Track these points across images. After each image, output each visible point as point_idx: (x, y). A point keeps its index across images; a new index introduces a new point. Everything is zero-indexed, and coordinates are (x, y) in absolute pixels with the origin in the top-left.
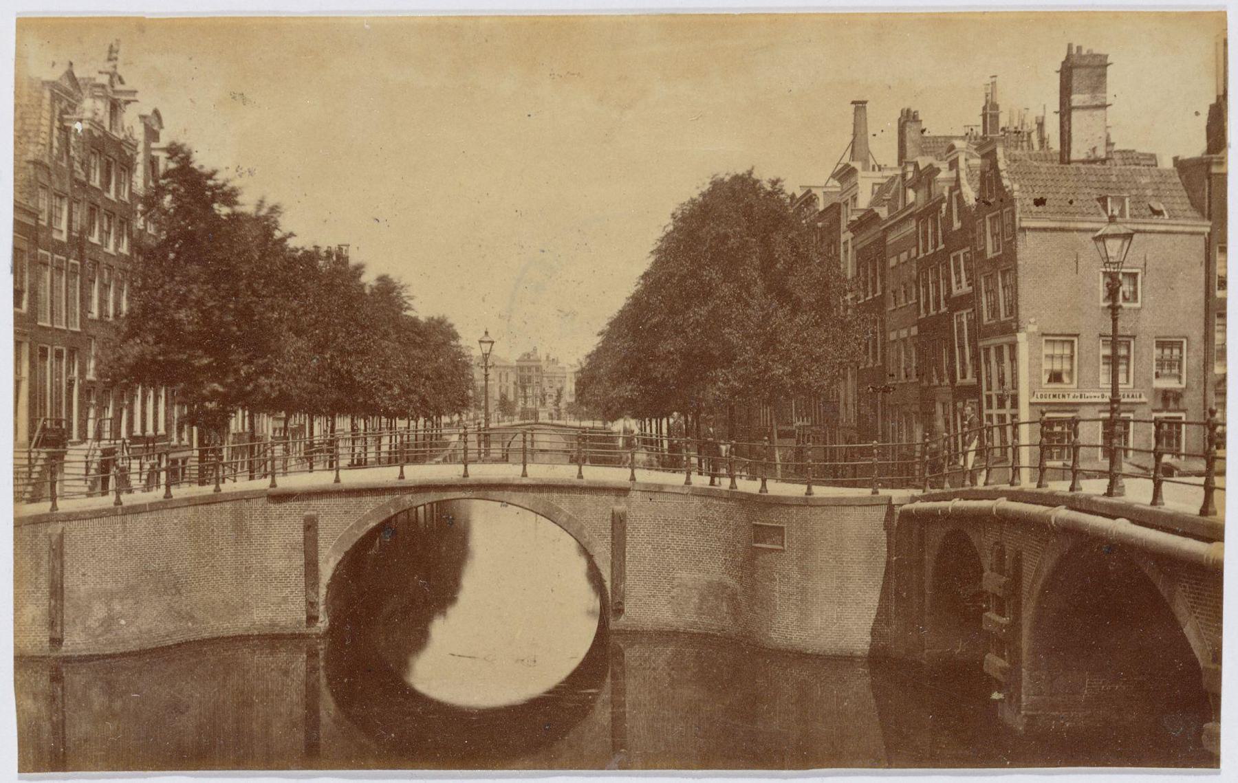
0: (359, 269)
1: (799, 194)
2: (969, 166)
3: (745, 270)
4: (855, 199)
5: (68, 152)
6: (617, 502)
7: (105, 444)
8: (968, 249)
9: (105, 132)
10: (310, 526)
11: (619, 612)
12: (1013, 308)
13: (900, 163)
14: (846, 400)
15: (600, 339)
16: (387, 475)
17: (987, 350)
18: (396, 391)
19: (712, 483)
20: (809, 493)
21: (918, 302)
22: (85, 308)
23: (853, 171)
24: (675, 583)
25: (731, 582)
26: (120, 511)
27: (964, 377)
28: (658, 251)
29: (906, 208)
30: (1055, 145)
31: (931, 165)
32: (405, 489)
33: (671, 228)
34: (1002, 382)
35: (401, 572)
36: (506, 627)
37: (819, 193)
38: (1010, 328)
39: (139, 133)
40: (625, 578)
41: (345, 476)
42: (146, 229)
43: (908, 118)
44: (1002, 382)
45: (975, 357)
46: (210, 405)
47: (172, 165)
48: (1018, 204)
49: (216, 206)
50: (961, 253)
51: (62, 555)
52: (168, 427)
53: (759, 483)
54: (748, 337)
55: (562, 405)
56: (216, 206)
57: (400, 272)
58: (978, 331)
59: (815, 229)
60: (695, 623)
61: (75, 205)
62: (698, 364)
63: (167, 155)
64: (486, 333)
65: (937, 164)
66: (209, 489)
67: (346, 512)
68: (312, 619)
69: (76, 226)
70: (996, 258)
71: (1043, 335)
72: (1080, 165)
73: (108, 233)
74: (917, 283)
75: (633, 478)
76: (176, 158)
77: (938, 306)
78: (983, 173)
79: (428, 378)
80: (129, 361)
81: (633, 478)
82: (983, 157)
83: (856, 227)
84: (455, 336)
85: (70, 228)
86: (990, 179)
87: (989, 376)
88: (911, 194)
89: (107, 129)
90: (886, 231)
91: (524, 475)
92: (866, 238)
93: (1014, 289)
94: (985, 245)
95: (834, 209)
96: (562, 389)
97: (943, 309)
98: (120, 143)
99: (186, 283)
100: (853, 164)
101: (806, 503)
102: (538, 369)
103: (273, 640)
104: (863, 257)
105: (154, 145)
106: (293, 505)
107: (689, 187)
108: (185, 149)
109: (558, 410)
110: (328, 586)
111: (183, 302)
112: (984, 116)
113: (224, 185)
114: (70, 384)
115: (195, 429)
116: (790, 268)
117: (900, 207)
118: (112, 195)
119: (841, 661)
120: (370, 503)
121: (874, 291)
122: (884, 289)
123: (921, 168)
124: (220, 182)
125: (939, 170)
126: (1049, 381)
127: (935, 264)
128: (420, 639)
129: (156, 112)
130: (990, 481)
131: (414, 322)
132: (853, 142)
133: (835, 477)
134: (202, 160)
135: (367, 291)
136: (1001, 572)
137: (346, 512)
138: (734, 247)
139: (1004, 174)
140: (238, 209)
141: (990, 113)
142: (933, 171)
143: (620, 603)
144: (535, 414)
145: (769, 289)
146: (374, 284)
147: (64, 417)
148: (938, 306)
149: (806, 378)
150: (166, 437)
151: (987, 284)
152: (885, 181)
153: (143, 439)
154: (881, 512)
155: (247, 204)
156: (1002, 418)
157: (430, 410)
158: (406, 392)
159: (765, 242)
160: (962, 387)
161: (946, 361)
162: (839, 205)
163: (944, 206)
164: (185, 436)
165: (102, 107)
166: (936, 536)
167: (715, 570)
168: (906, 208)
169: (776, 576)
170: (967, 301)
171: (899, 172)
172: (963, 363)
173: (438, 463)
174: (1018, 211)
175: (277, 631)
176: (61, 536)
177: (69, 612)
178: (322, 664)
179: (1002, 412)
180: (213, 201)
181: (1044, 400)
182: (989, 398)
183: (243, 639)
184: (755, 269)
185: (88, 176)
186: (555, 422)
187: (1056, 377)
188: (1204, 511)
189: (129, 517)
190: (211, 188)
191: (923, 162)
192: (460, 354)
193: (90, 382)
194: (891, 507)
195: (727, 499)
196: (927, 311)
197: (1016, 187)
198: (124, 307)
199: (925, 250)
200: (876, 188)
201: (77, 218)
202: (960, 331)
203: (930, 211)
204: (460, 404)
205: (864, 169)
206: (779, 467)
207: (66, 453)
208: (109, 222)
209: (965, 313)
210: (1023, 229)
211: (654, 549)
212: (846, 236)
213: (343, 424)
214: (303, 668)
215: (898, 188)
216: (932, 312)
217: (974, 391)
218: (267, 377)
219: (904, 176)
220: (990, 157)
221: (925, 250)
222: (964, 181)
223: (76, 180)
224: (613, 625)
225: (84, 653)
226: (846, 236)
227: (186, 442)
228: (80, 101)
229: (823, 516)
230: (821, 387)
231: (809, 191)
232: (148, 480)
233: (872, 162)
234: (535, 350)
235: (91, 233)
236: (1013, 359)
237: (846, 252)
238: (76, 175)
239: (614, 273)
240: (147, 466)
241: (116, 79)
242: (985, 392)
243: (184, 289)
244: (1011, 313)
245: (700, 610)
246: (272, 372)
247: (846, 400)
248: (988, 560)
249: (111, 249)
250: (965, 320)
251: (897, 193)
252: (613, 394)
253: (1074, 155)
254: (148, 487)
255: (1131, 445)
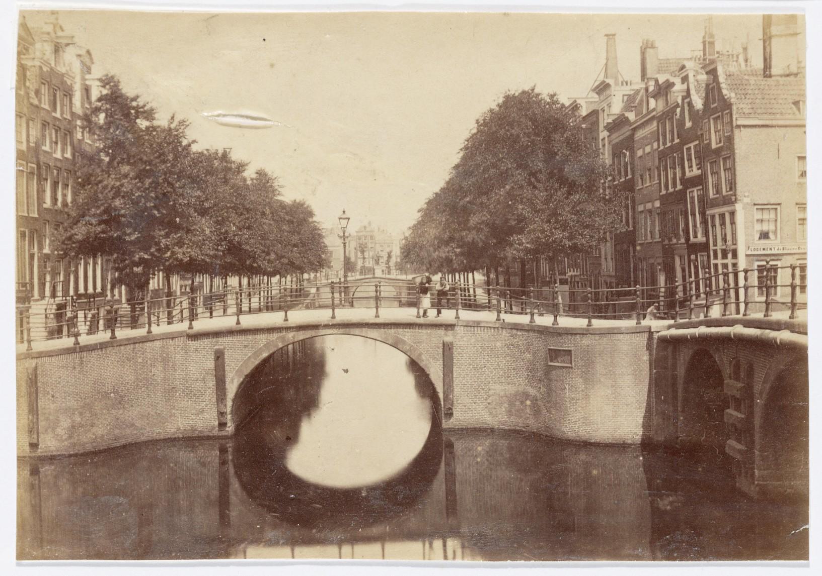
0: (241, 167)
1: (567, 104)
2: (697, 81)
3: (533, 162)
4: (609, 106)
5: (24, 84)
6: (446, 335)
7: (59, 300)
8: (697, 142)
9: (52, 69)
10: (219, 356)
11: (450, 415)
12: (732, 185)
13: (643, 80)
14: (606, 255)
15: (419, 214)
16: (274, 318)
17: (713, 217)
18: (273, 256)
19: (638, 323)
20: (589, 325)
21: (660, 183)
22: (41, 200)
23: (607, 86)
24: (491, 392)
25: (532, 392)
26: (78, 350)
27: (696, 237)
28: (466, 148)
29: (649, 112)
30: (759, 64)
31: (667, 80)
32: (288, 329)
33: (475, 131)
34: (724, 240)
35: (281, 390)
36: (358, 430)
37: (581, 102)
38: (729, 201)
39: (77, 67)
40: (453, 391)
41: (244, 322)
42: (83, 139)
43: (646, 47)
44: (724, 240)
45: (704, 222)
46: (138, 270)
47: (105, 92)
48: (734, 108)
49: (138, 121)
50: (692, 145)
51: (36, 383)
52: (104, 288)
53: (528, 317)
54: (537, 211)
55: (392, 263)
56: (138, 121)
57: (271, 169)
58: (705, 203)
59: (580, 128)
60: (506, 422)
61: (31, 123)
62: (502, 233)
63: (99, 83)
64: (344, 212)
65: (672, 80)
66: (141, 332)
67: (245, 346)
68: (222, 425)
69: (32, 139)
70: (719, 148)
71: (755, 204)
72: (779, 78)
73: (56, 143)
74: (658, 168)
75: (457, 317)
76: (108, 87)
77: (675, 185)
78: (707, 85)
79: (295, 246)
80: (79, 237)
81: (457, 317)
82: (707, 73)
83: (613, 127)
84: (311, 214)
85: (28, 141)
86: (712, 90)
87: (715, 237)
88: (652, 103)
89: (53, 65)
90: (635, 130)
91: (377, 316)
92: (617, 137)
93: (732, 170)
94: (710, 139)
95: (594, 114)
96: (391, 252)
97: (679, 187)
98: (63, 75)
99: (119, 179)
100: (608, 81)
101: (583, 333)
102: (372, 237)
103: (192, 440)
104: (617, 153)
105: (87, 76)
106: (206, 342)
107: (491, 101)
108: (115, 79)
109: (389, 268)
110: (233, 401)
111: (117, 193)
112: (704, 43)
113: (145, 106)
114: (32, 256)
115: (123, 287)
116: (566, 160)
117: (645, 112)
118: (58, 115)
119: (619, 447)
120: (262, 339)
121: (626, 175)
122: (633, 174)
123: (660, 83)
124: (141, 104)
125: (673, 84)
126: (760, 238)
127: (669, 157)
128: (292, 438)
129: (88, 52)
130: (727, 313)
131: (283, 206)
132: (606, 64)
133: (601, 312)
134: (128, 89)
135: (249, 182)
136: (737, 379)
137: (245, 346)
138: (525, 146)
139: (723, 86)
140: (155, 123)
141: (708, 44)
142: (669, 85)
143: (450, 409)
144: (372, 270)
145: (551, 175)
146: (254, 176)
147: (27, 281)
148: (675, 185)
149: (580, 241)
150: (103, 293)
151: (712, 168)
152: (632, 92)
153: (86, 295)
154: (643, 339)
155: (162, 120)
156: (725, 266)
157: (296, 268)
158: (279, 257)
159: (548, 140)
160: (695, 245)
161: (682, 225)
162: (598, 111)
163: (678, 110)
164: (116, 291)
165: (48, 49)
166: (685, 356)
167: (520, 384)
168: (649, 112)
169: (567, 387)
170: (699, 181)
171: (644, 86)
172: (695, 226)
173: (300, 309)
174: (734, 112)
175: (196, 434)
176: (36, 369)
177: (42, 424)
178: (230, 457)
179: (725, 261)
180: (137, 117)
181: (756, 253)
182: (715, 252)
183: (171, 441)
184: (540, 161)
185: (40, 101)
186: (388, 276)
187: (764, 235)
188: (531, 322)
189: (85, 354)
190: (134, 108)
191: (662, 79)
192: (316, 229)
193: (46, 254)
194: (651, 333)
195: (528, 331)
196: (667, 188)
197: (733, 95)
198: (69, 199)
199: (664, 143)
200: (626, 98)
201: (33, 132)
202: (693, 203)
203: (668, 114)
204: (320, 263)
205: (616, 84)
206: (561, 306)
207: (30, 307)
208: (56, 134)
209: (695, 190)
210: (738, 127)
211: (475, 368)
212: (604, 134)
213: (233, 281)
214: (217, 460)
215: (642, 97)
216: (671, 190)
217: (705, 247)
218: (181, 247)
219: (647, 90)
220: (713, 73)
221: (664, 143)
222: (693, 92)
223: (32, 104)
224: (446, 424)
225: (55, 453)
226: (604, 134)
227: (117, 297)
228: (33, 44)
229: (601, 342)
230: (590, 247)
231: (575, 101)
232: (90, 326)
233: (620, 80)
234: (370, 223)
235: (44, 143)
236: (733, 223)
237: (604, 146)
238: (31, 101)
239: (433, 167)
240: (90, 316)
241: (58, 29)
242: (712, 247)
243: (118, 184)
244: (731, 189)
245: (509, 413)
246: (184, 244)
247: (606, 255)
248: (727, 371)
249: (58, 155)
250: (695, 194)
251: (642, 100)
252: (435, 255)
253: (774, 71)
254: (90, 332)
255: (779, 283)
